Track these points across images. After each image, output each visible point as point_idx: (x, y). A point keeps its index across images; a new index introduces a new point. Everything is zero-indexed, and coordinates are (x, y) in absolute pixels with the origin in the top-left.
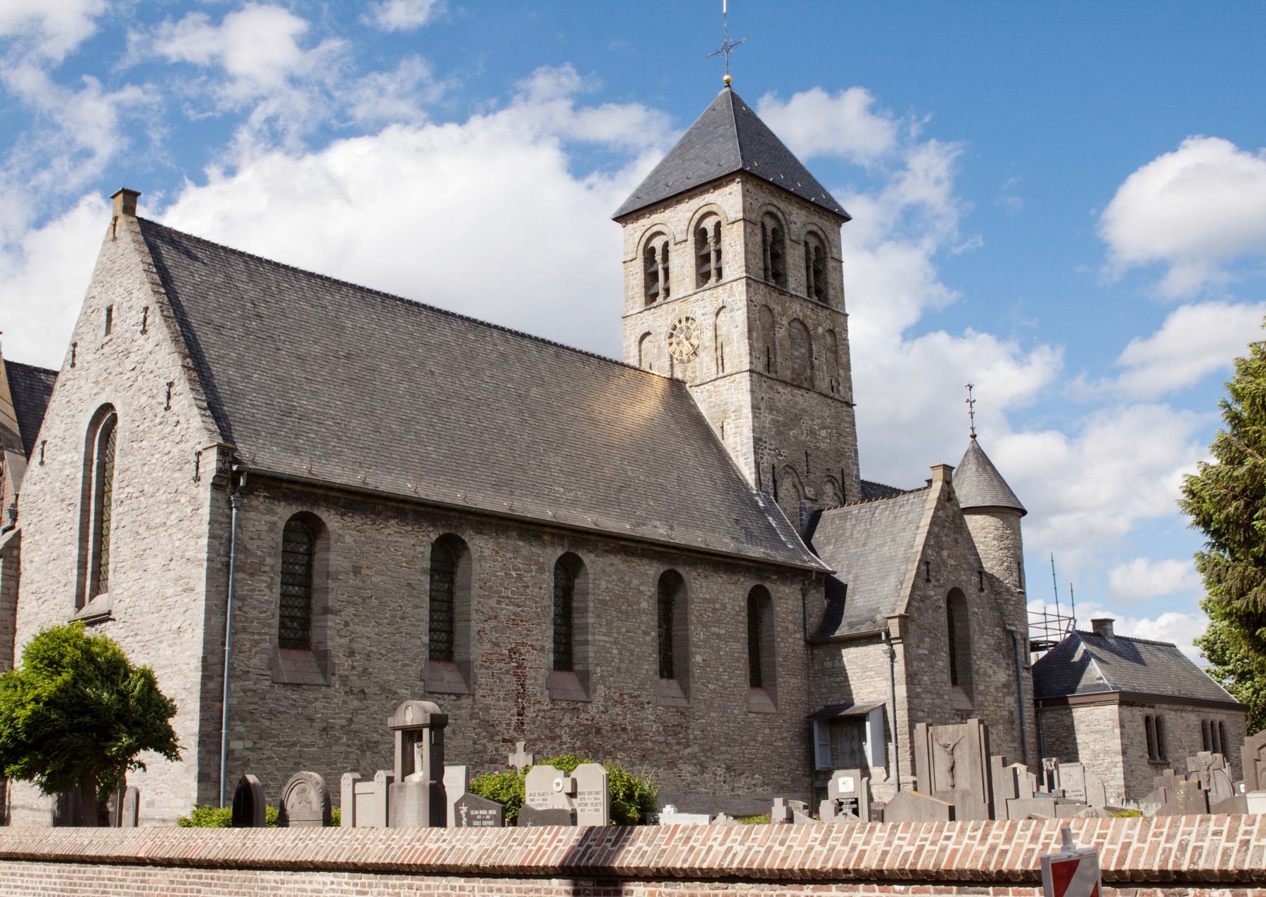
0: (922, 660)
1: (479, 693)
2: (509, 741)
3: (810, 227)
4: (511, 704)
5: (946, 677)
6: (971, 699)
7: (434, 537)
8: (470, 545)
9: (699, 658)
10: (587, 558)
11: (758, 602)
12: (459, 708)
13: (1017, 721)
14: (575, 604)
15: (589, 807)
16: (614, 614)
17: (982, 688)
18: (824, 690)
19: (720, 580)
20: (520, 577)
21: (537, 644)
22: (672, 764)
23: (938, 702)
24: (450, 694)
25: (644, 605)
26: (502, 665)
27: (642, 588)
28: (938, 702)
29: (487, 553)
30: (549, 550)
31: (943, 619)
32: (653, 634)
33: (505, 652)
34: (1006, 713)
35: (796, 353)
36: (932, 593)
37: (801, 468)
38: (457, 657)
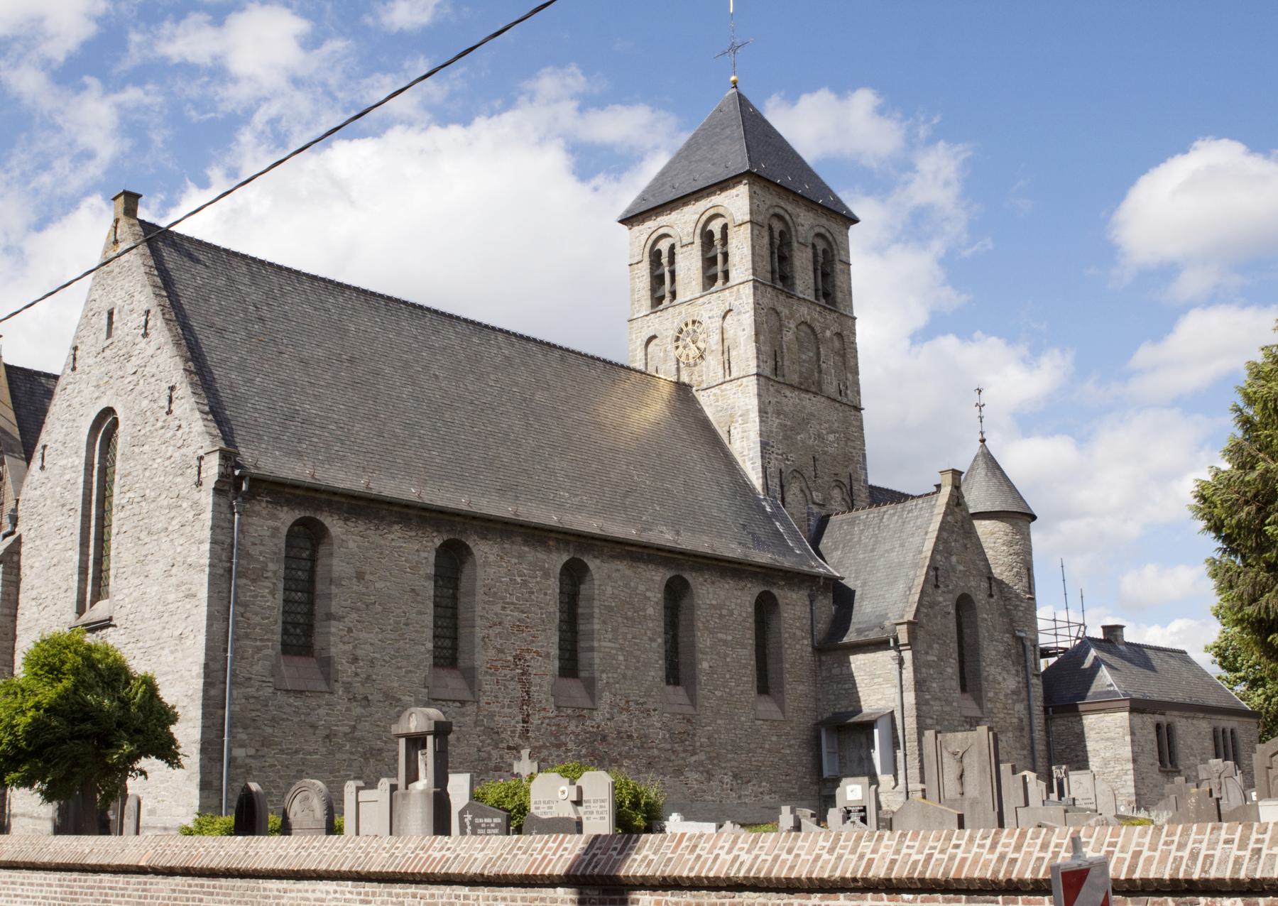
0: (930, 667)
1: (484, 700)
2: (514, 748)
3: (818, 230)
4: (516, 711)
5: (955, 683)
6: (980, 706)
7: (438, 542)
8: (474, 550)
9: (705, 665)
10: (593, 564)
11: (765, 608)
12: (463, 715)
13: (1027, 729)
14: (580, 611)
15: (595, 815)
16: (620, 620)
17: (991, 694)
18: (832, 697)
19: (727, 586)
20: (525, 583)
21: (543, 651)
22: (678, 772)
23: (947, 709)
24: (454, 701)
25: (650, 611)
26: (507, 672)
27: (648, 594)
28: (947, 709)
29: (492, 558)
30: (554, 556)
31: (953, 626)
32: (660, 640)
33: (510, 658)
34: (1015, 720)
35: (804, 357)
36: (941, 599)
37: (809, 472)
38: (461, 663)
